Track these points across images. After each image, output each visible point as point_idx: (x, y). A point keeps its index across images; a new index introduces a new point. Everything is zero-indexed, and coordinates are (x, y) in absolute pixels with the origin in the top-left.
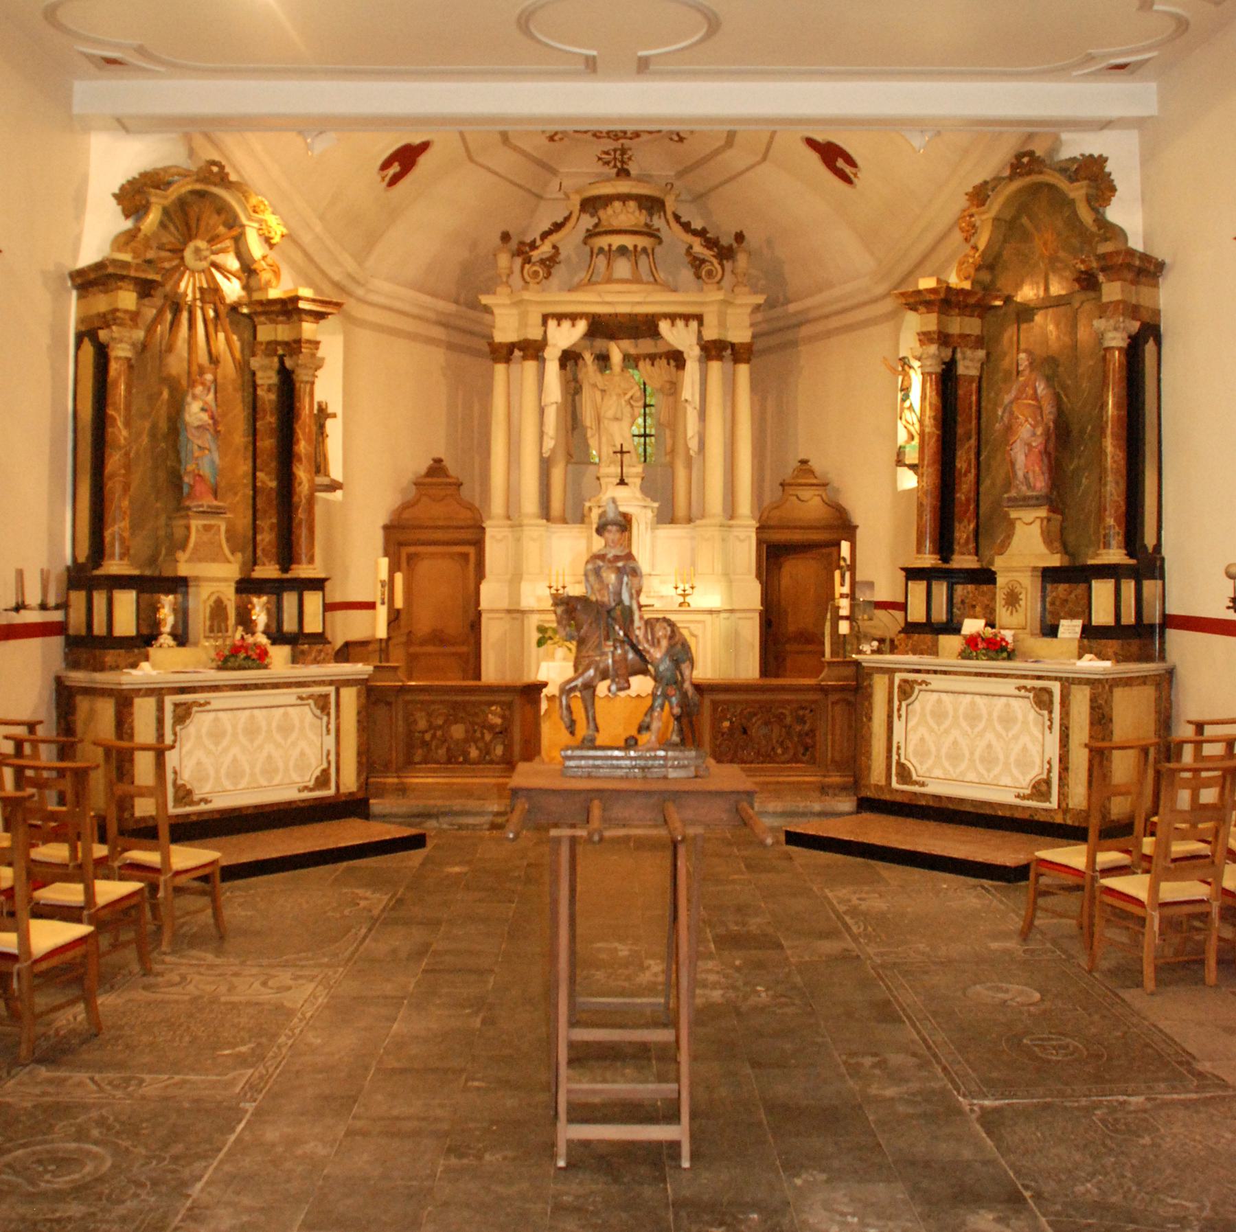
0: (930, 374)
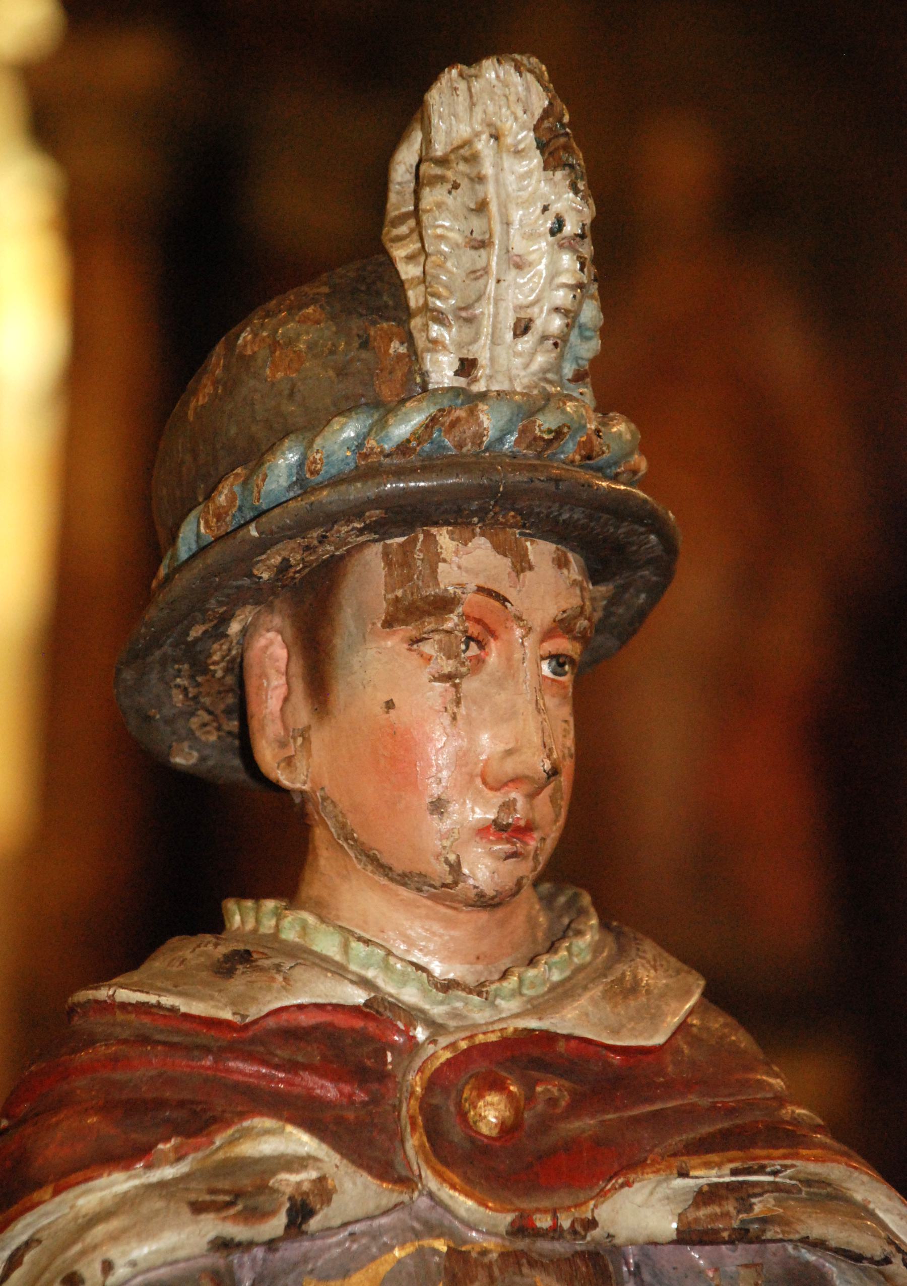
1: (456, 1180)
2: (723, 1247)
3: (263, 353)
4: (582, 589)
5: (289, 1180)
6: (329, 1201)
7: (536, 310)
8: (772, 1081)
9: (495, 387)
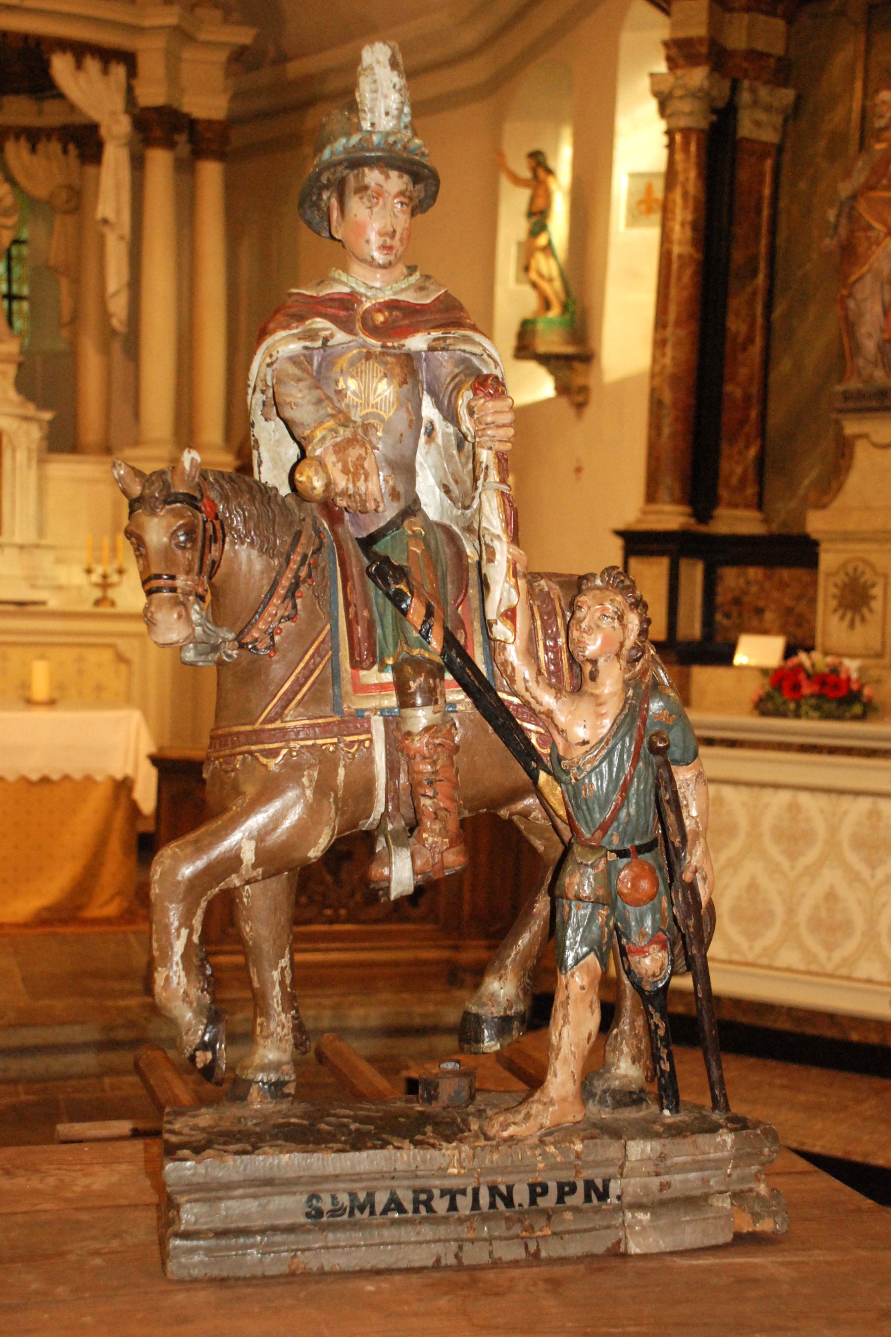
0: (686, 132)
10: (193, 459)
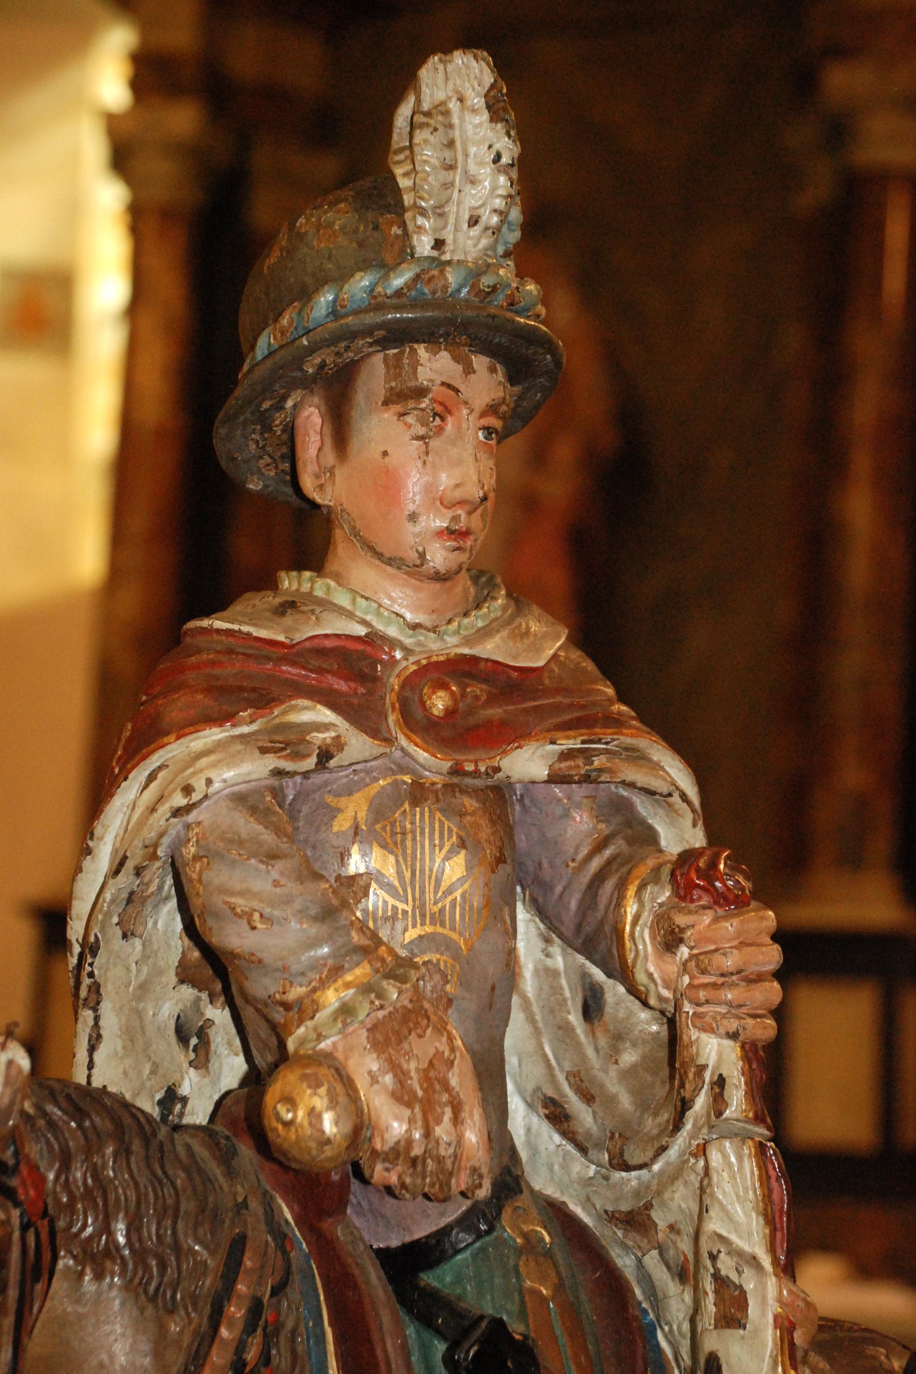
1: (418, 741)
2: (574, 785)
3: (312, 231)
4: (504, 387)
5: (318, 737)
6: (342, 750)
7: (482, 210)
8: (607, 690)
9: (456, 258)
10: (10, 1063)
